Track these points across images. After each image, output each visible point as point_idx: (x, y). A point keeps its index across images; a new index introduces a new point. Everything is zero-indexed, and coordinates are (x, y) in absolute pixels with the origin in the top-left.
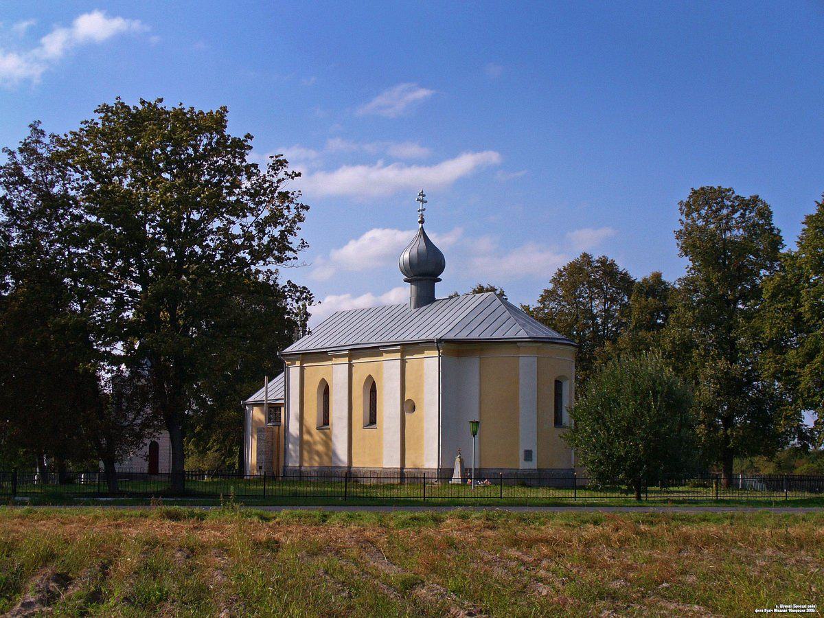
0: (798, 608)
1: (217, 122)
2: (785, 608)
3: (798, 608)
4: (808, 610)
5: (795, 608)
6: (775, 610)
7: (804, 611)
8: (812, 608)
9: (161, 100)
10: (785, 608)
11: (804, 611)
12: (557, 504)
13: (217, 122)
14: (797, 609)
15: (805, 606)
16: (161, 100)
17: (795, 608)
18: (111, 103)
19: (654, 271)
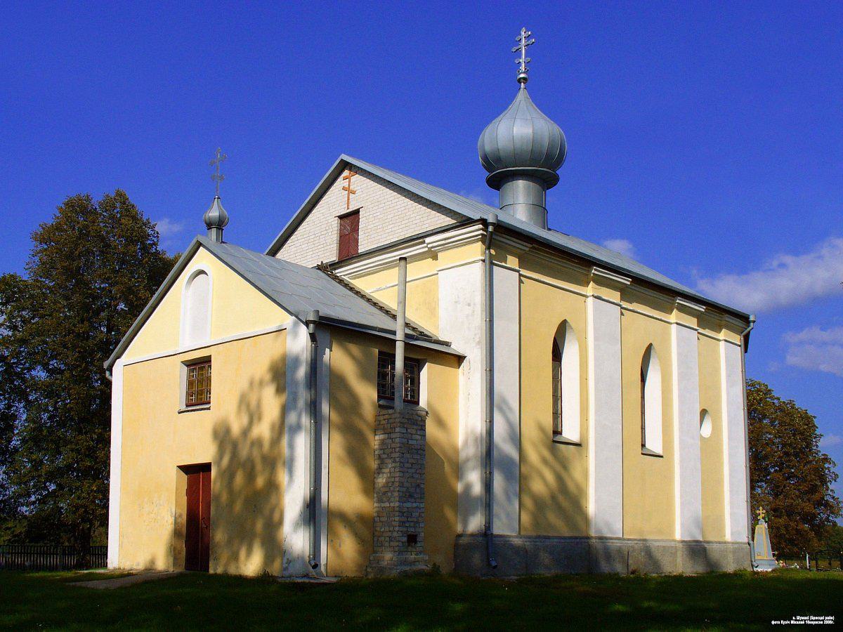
0: (815, 620)
1: (196, 473)
2: (802, 620)
3: (815, 620)
4: (826, 622)
5: (812, 620)
6: (792, 622)
7: (822, 622)
8: (829, 620)
9: (815, 417)
10: (802, 620)
11: (822, 622)
12: (202, 532)
13: (196, 473)
14: (813, 620)
15: (822, 618)
16: (815, 417)
17: (812, 620)
18: (40, 230)
19: (73, 194)
